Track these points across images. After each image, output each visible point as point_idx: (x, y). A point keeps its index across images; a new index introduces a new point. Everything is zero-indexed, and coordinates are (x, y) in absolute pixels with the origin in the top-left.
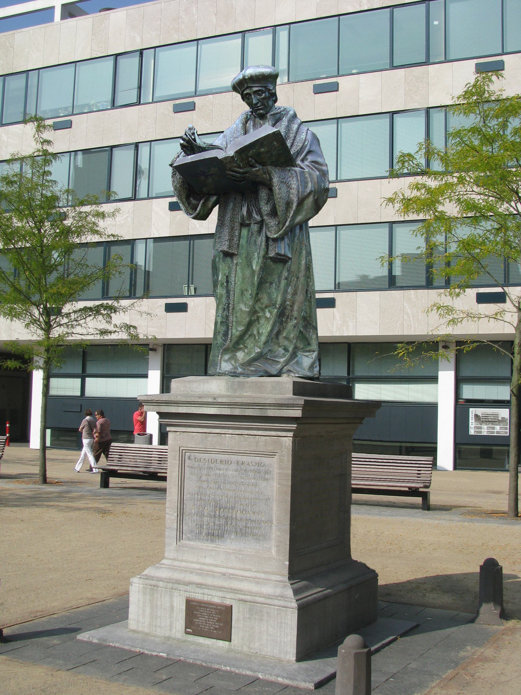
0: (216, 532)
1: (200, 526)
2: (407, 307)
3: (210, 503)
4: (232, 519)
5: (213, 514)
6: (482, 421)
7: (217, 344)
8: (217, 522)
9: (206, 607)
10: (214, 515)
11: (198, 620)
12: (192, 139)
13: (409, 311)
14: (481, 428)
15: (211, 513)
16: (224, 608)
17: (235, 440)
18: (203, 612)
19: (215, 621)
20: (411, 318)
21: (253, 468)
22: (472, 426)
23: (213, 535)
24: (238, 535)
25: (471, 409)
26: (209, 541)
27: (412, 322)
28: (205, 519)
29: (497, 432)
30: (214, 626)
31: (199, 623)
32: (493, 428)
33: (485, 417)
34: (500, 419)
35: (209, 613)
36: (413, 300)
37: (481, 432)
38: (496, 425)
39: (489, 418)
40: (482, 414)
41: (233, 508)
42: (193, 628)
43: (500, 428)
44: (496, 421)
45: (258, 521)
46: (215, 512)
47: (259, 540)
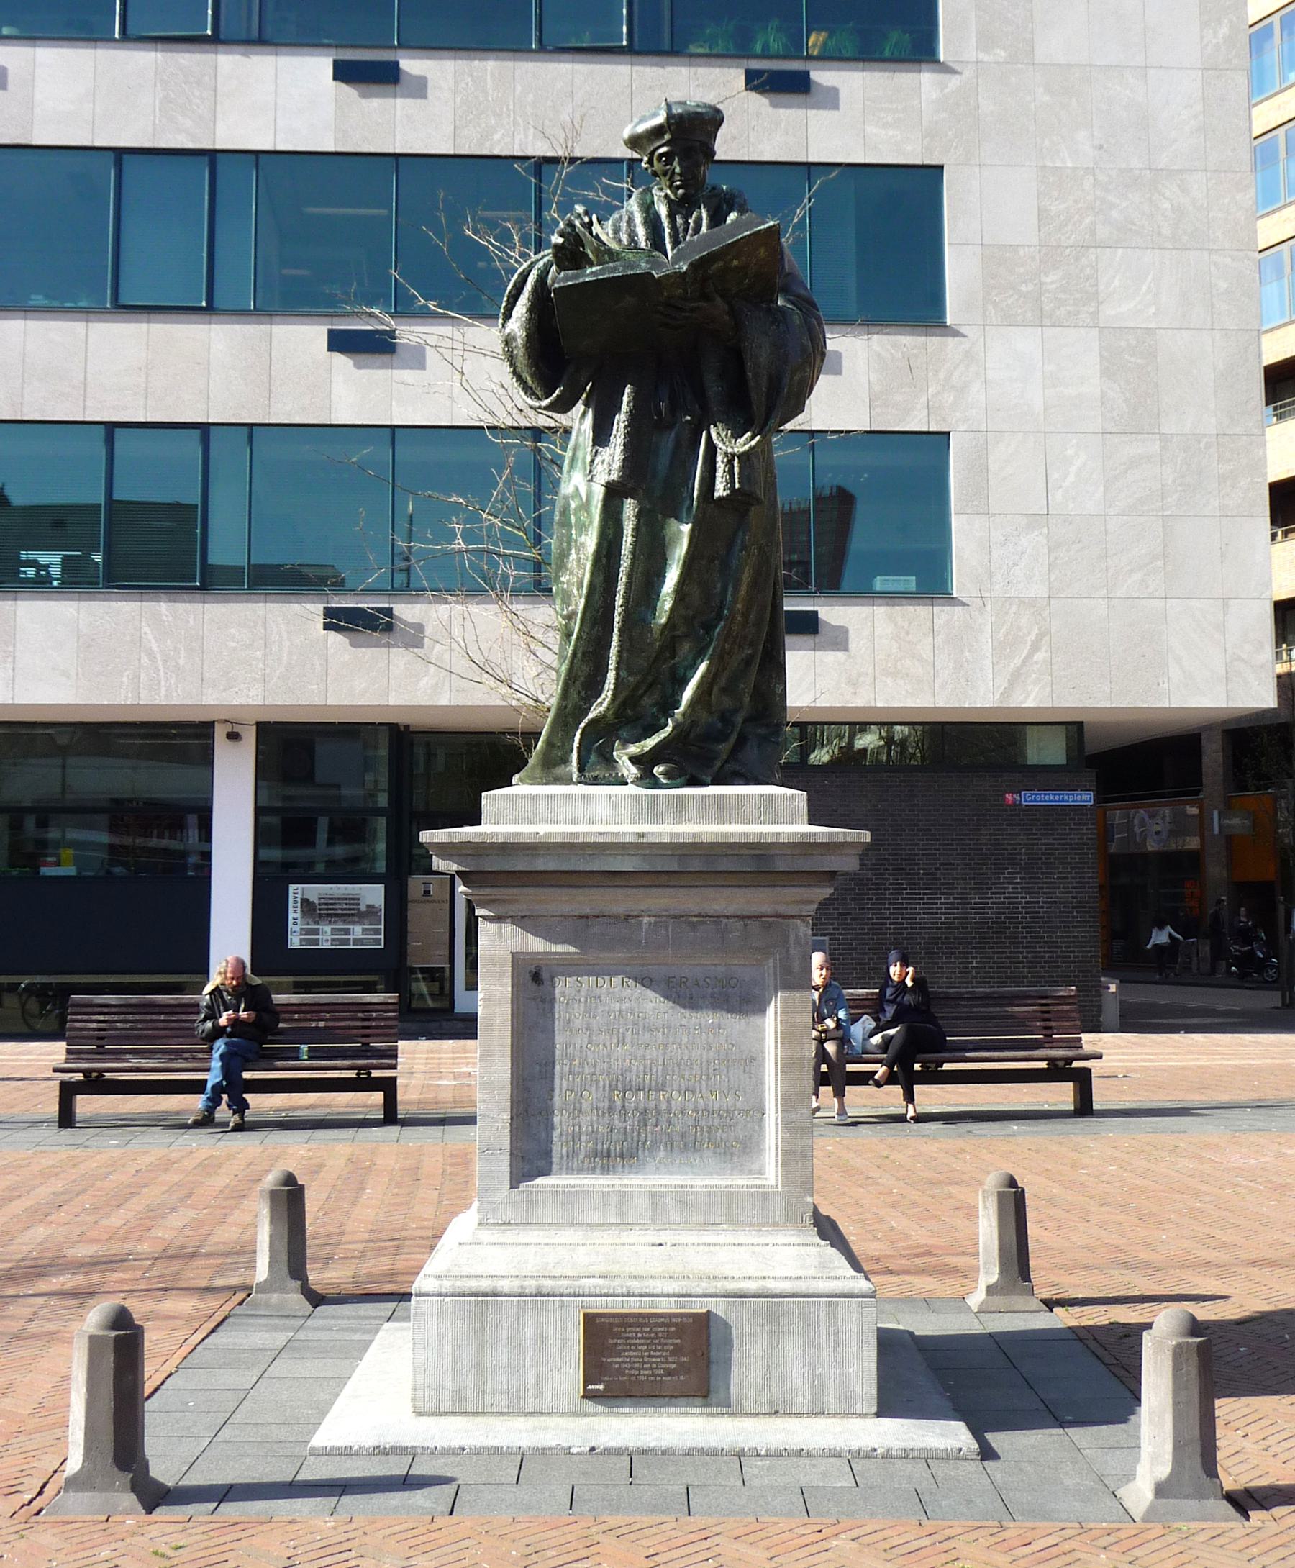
0: (617, 1148)
1: (570, 1138)
2: (150, 637)
3: (598, 1081)
4: (658, 1112)
5: (606, 1105)
6: (320, 915)
7: (566, 707)
8: (617, 1124)
9: (642, 1325)
10: (610, 1108)
11: (621, 1360)
12: (583, 225)
13: (154, 647)
14: (316, 932)
15: (601, 1105)
16: (691, 1320)
17: (667, 931)
18: (632, 1338)
19: (668, 1354)
20: (160, 663)
21: (710, 991)
22: (297, 928)
23: (609, 1156)
24: (676, 1150)
25: (292, 887)
26: (598, 1171)
27: (162, 673)
28: (585, 1120)
29: (356, 941)
30: (663, 1366)
31: (624, 1365)
32: (347, 932)
33: (326, 904)
34: (363, 908)
35: (648, 1339)
36: (165, 618)
37: (316, 942)
38: (354, 923)
39: (338, 907)
40: (320, 899)
41: (660, 1088)
42: (606, 1379)
43: (364, 930)
44: (353, 915)
45: (727, 1111)
46: (612, 1101)
47: (732, 1154)
